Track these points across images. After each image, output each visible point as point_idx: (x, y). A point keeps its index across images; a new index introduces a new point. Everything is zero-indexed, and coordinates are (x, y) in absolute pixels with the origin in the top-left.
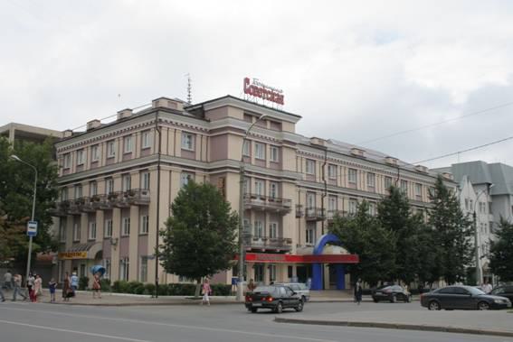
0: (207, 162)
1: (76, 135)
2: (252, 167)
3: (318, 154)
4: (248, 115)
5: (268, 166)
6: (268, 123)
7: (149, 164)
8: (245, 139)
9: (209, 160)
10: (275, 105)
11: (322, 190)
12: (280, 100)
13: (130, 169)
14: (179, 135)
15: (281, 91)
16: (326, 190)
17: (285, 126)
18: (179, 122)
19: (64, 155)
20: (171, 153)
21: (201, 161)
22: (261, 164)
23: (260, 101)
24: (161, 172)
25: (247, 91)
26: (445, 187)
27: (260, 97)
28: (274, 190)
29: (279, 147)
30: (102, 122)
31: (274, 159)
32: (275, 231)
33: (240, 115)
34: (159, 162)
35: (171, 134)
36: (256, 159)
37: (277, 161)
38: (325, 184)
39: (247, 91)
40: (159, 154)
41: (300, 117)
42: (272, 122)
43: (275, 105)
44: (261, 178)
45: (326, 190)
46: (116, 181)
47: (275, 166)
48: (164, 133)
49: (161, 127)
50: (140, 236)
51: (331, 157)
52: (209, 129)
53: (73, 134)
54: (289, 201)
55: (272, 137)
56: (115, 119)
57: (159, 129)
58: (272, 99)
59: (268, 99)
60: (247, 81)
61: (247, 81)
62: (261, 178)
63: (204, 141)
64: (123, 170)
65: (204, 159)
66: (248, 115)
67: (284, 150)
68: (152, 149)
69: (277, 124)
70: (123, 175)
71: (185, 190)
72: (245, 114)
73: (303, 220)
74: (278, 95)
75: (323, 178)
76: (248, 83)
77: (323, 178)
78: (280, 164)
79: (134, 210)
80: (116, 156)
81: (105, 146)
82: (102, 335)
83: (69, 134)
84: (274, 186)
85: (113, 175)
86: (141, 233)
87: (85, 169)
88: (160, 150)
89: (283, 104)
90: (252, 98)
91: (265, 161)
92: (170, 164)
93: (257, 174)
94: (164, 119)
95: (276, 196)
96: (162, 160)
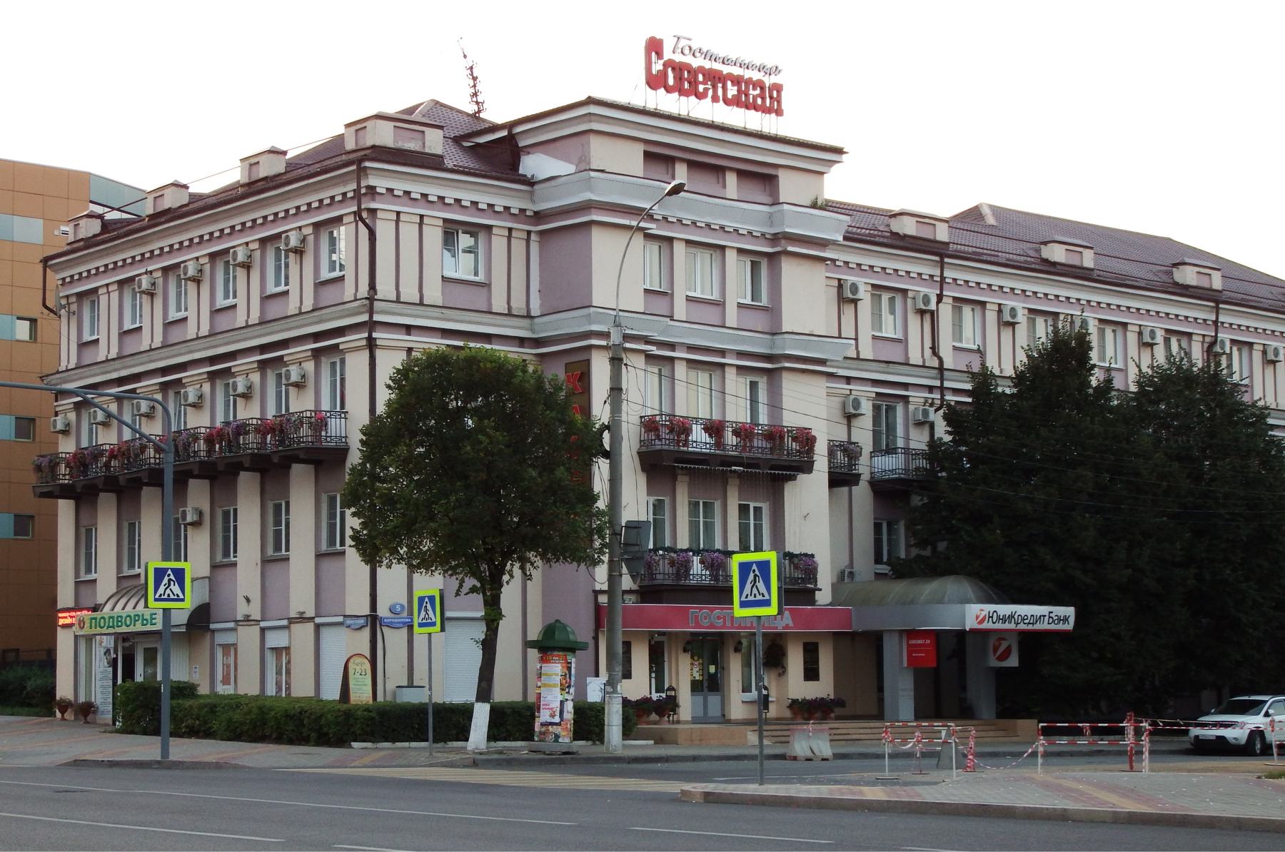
0: (529, 316)
1: (201, 207)
4: (659, 158)
5: (732, 317)
6: (731, 179)
7: (340, 331)
8: (649, 237)
9: (535, 309)
11: (931, 389)
13: (284, 344)
15: (777, 70)
16: (942, 389)
17: (790, 186)
18: (434, 191)
19: (80, 296)
20: (409, 293)
21: (510, 314)
22: (711, 315)
24: (379, 354)
25: (655, 81)
27: (700, 96)
29: (770, 256)
30: (194, 189)
31: (755, 294)
32: (758, 529)
33: (631, 159)
34: (371, 325)
36: (689, 299)
37: (764, 301)
38: (941, 369)
39: (655, 81)
40: (371, 299)
41: (839, 151)
42: (741, 174)
46: (351, 359)
47: (759, 321)
48: (384, 230)
49: (373, 212)
52: (531, 207)
53: (106, 226)
55: (744, 228)
57: (366, 219)
59: (727, 102)
60: (654, 46)
61: (654, 46)
63: (518, 246)
65: (518, 304)
66: (659, 158)
67: (789, 270)
72: (648, 155)
73: (862, 492)
74: (760, 85)
76: (660, 55)
78: (773, 311)
80: (349, 274)
82: (766, 837)
83: (277, 167)
89: (779, 112)
91: (720, 304)
92: (408, 329)
93: (691, 348)
94: (381, 184)
95: (763, 419)
96: (376, 318)
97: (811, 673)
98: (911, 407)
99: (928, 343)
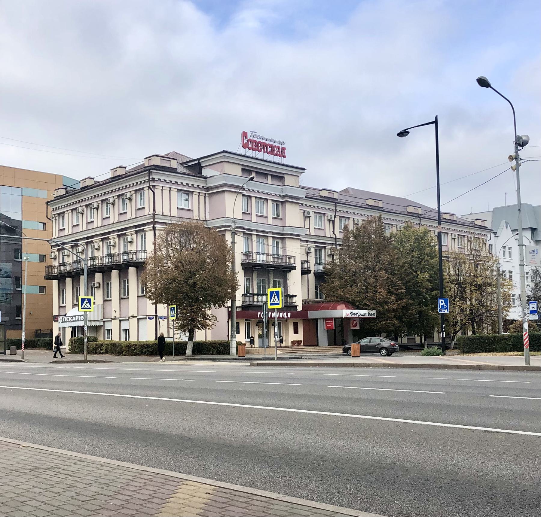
2: (255, 223)
3: (327, 207)
6: (270, 178)
8: (243, 195)
10: (276, 159)
12: (281, 152)
14: (174, 194)
17: (288, 180)
18: (174, 180)
19: (59, 214)
23: (260, 155)
25: (245, 146)
26: (364, 344)
27: (259, 151)
28: (278, 247)
30: (96, 179)
33: (237, 171)
35: (166, 192)
38: (336, 238)
39: (245, 146)
40: (154, 214)
41: (304, 169)
42: (273, 176)
43: (276, 159)
44: (263, 235)
45: (336, 245)
48: (158, 192)
49: (154, 186)
50: (138, 297)
51: (342, 209)
54: (293, 257)
56: (109, 176)
58: (272, 153)
60: (244, 135)
61: (244, 135)
62: (263, 235)
64: (119, 230)
66: (246, 170)
68: (147, 208)
69: (279, 177)
70: (103, 240)
71: (7, 319)
72: (243, 170)
75: (334, 232)
76: (246, 137)
77: (334, 232)
79: (132, 271)
81: (70, 214)
84: (278, 243)
85: (110, 236)
86: (140, 294)
87: (129, 218)
88: (154, 210)
89: (285, 157)
90: (249, 153)
94: (157, 177)
96: (156, 220)
97: (296, 332)
98: (327, 250)
99: (332, 230)
